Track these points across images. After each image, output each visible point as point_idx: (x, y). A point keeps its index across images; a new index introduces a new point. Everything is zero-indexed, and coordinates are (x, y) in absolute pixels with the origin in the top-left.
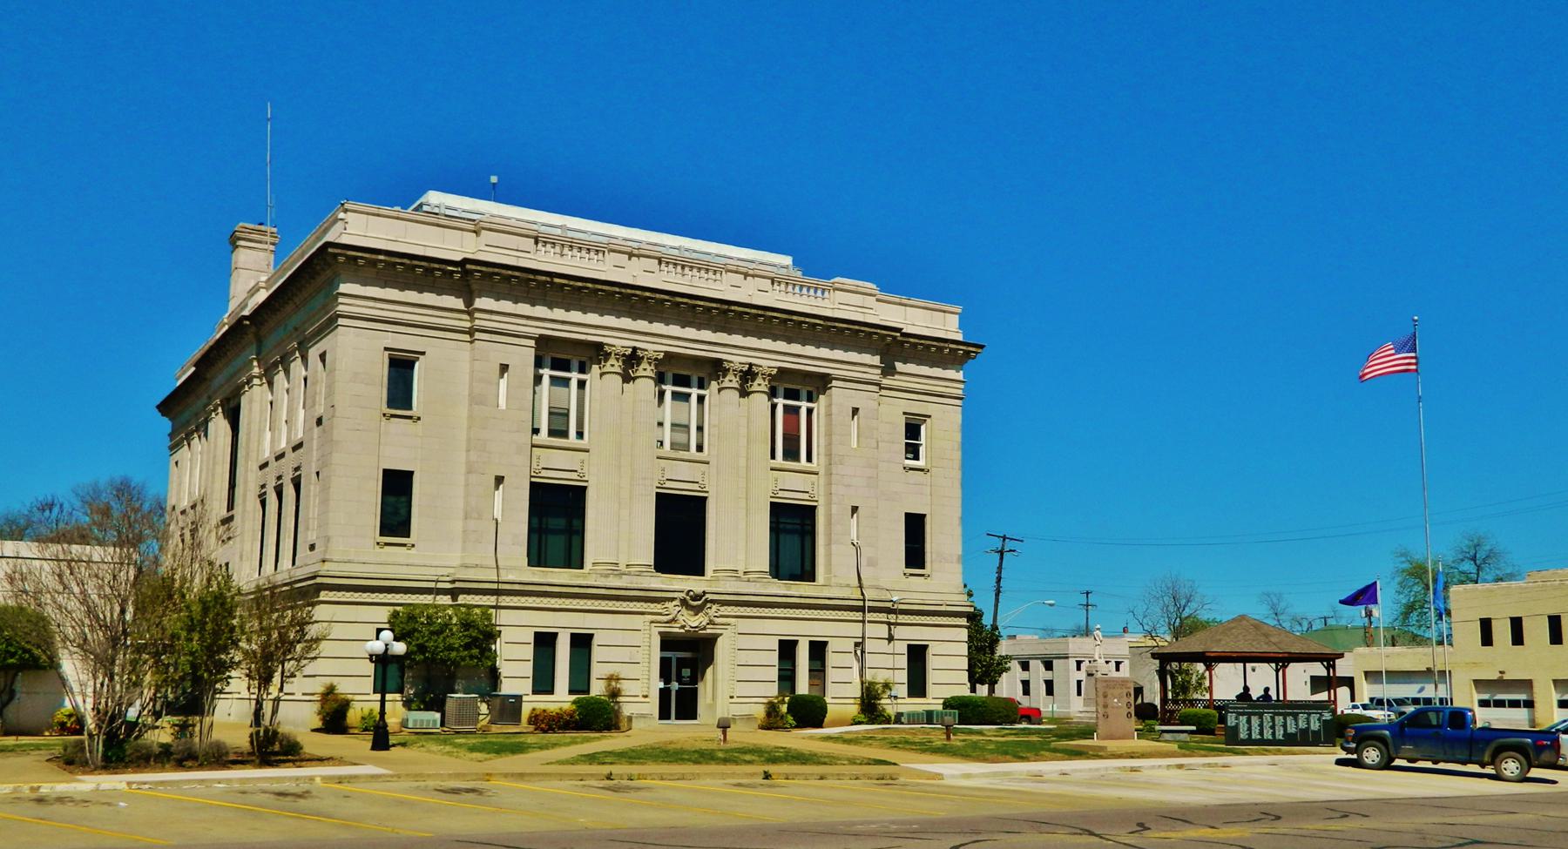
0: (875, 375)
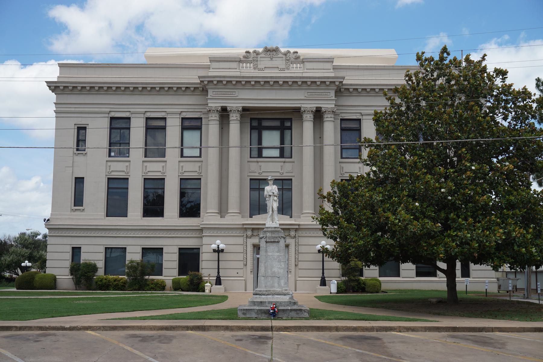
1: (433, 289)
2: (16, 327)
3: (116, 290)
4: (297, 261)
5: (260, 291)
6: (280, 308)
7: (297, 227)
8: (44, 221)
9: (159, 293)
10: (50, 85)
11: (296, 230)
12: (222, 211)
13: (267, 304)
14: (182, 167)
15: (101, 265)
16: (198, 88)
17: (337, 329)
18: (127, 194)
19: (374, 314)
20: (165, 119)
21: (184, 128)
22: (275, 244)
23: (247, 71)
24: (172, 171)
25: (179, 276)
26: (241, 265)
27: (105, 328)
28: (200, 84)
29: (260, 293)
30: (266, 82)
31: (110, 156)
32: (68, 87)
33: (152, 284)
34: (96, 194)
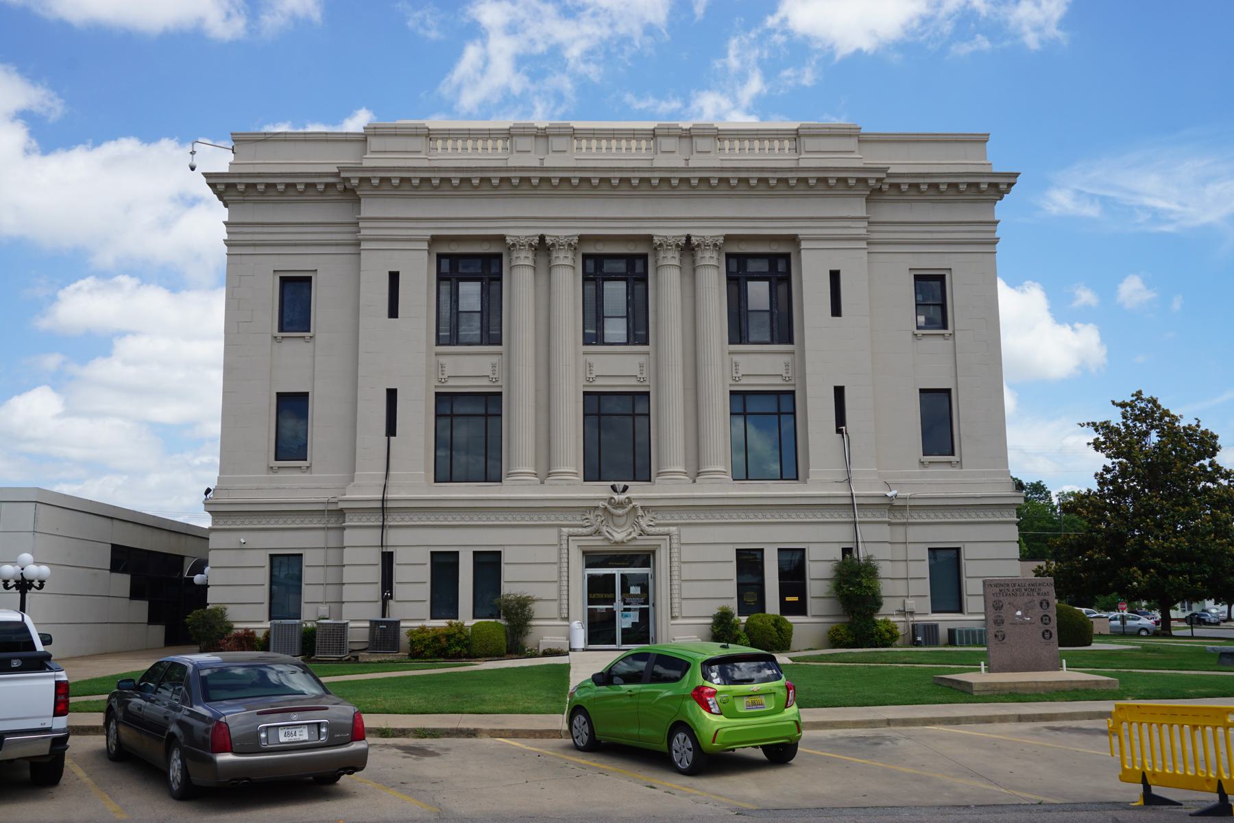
0: (860, 229)
10: (213, 181)
17: (403, 733)
25: (432, 618)
30: (523, 180)
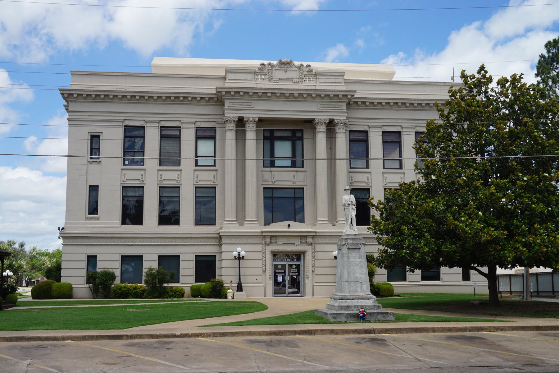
1: (420, 292)
2: (127, 336)
3: (136, 298)
4: (314, 266)
5: (345, 296)
6: (368, 312)
7: (314, 234)
8: (59, 229)
9: (176, 301)
11: (313, 237)
12: (241, 217)
13: (353, 309)
14: (197, 175)
15: (118, 273)
16: (213, 98)
18: (179, 202)
19: (457, 317)
20: (179, 128)
21: (198, 138)
22: (356, 251)
23: (262, 83)
24: (187, 180)
26: (260, 271)
27: (215, 335)
28: (215, 94)
29: (345, 297)
31: (124, 164)
32: (82, 95)
33: (171, 291)
34: (111, 204)
